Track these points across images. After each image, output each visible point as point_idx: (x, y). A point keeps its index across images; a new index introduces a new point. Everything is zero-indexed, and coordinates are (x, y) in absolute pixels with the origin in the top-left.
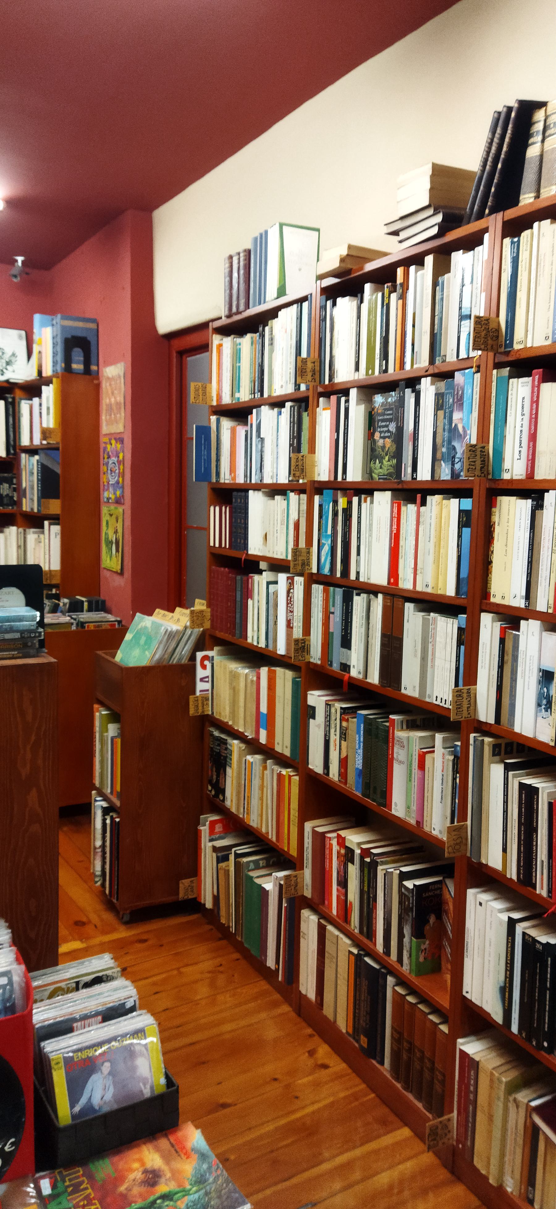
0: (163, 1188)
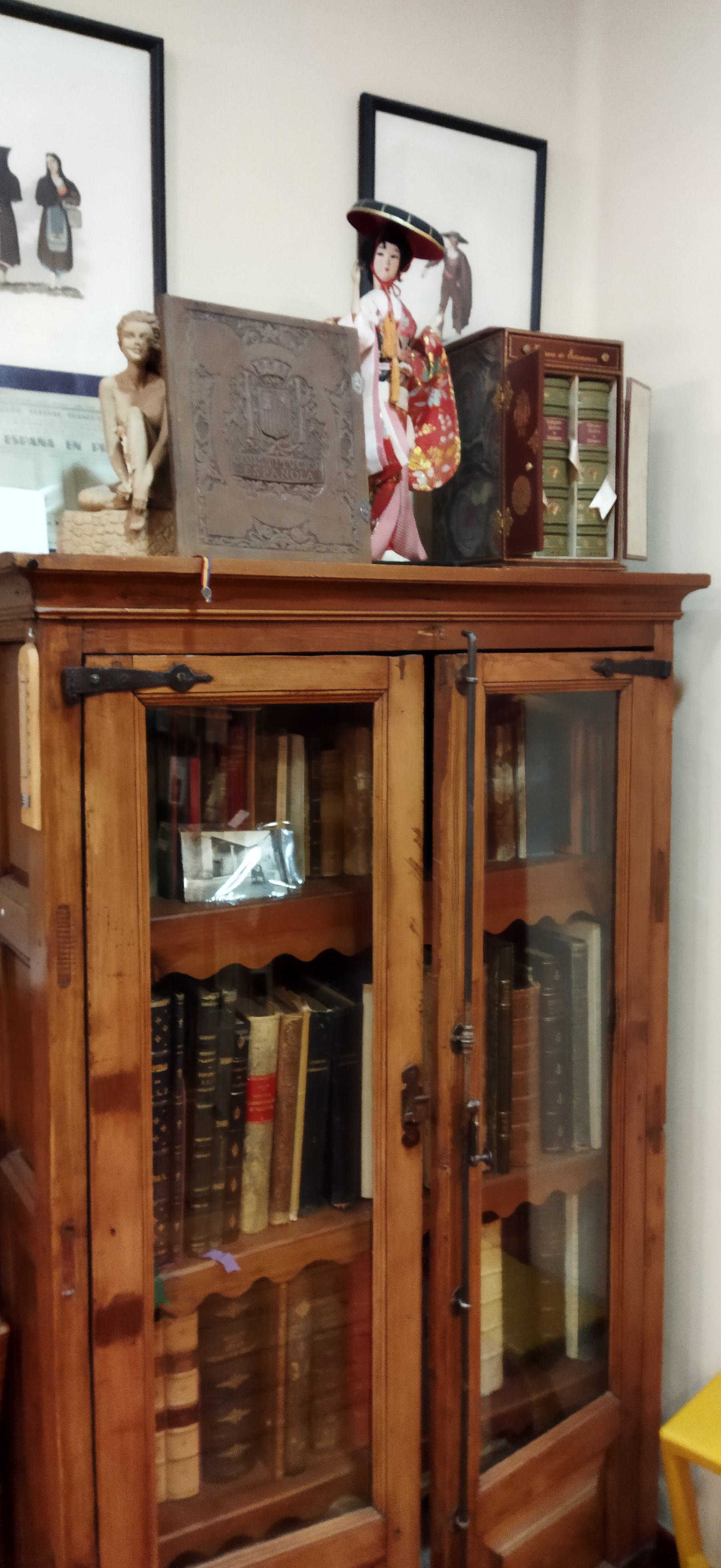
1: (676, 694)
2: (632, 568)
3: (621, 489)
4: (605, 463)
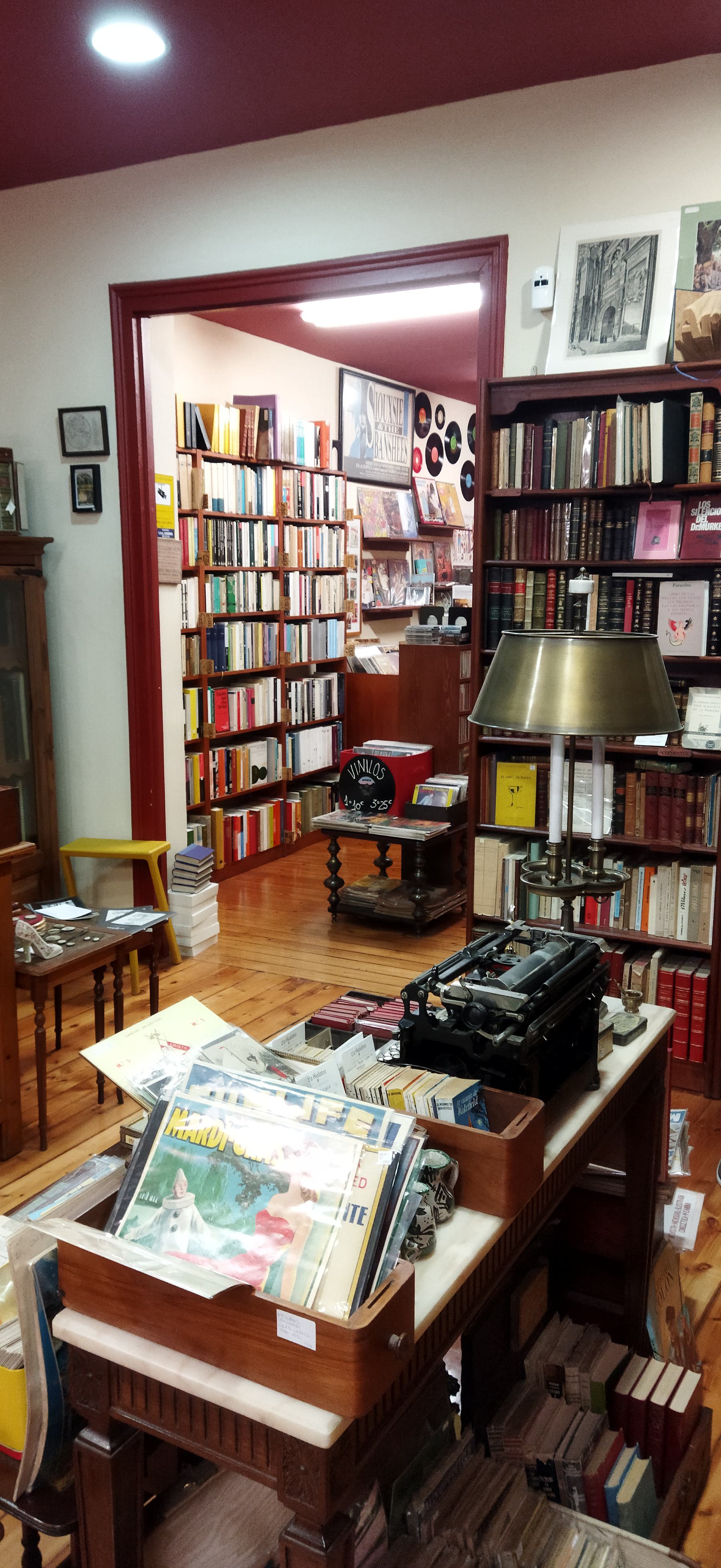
1: (44, 584)
2: (24, 534)
3: (17, 504)
4: (9, 494)
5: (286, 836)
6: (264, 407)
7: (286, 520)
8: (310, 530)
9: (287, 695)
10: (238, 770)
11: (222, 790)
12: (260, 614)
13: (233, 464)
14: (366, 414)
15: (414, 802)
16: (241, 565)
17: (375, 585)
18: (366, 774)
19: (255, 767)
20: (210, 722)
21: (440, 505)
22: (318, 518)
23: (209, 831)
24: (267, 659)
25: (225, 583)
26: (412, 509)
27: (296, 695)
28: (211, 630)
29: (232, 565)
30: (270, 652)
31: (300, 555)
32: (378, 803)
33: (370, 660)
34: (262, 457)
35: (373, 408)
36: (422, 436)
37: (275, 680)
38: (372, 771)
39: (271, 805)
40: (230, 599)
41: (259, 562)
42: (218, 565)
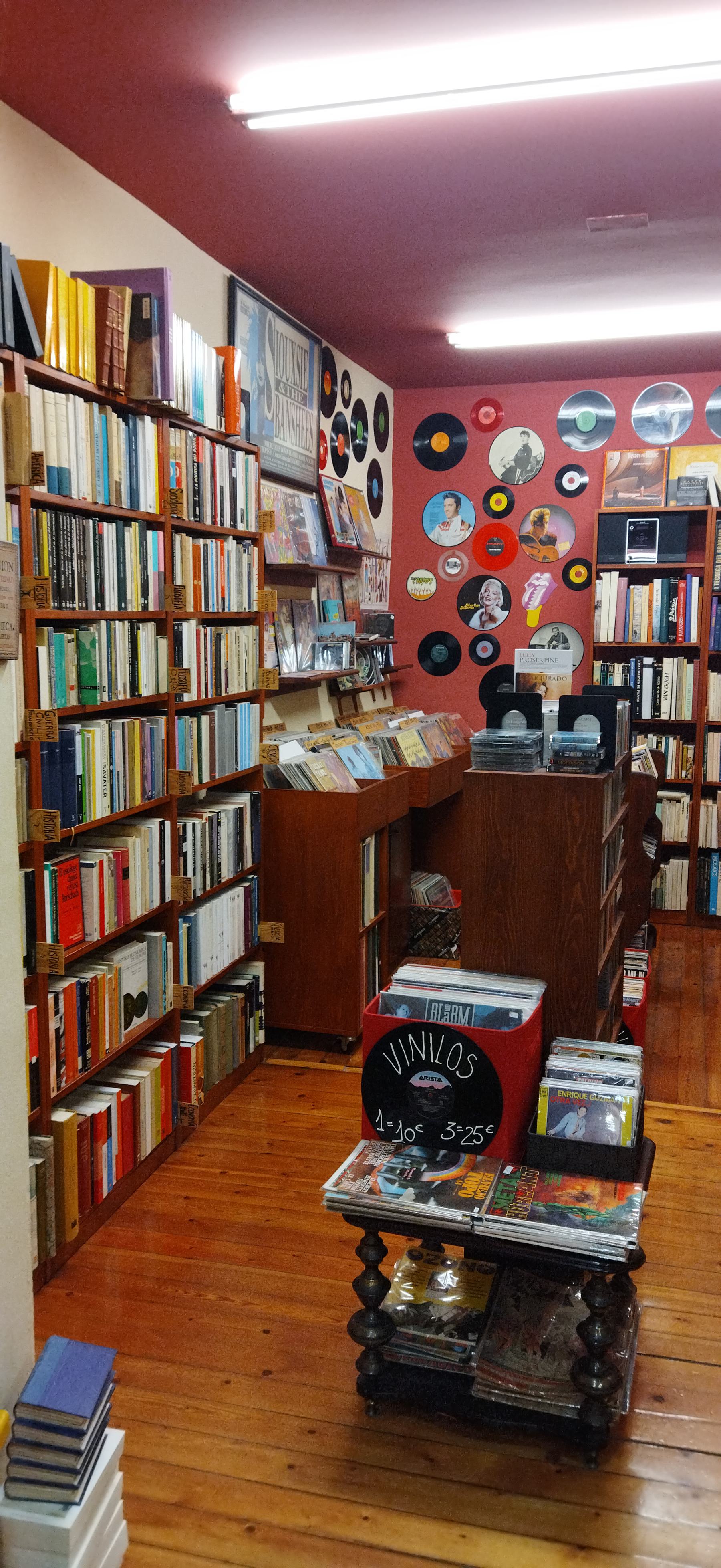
0: (585, 1205)
5: (182, 1112)
6: (142, 290)
7: (176, 522)
8: (212, 544)
9: (181, 848)
10: (101, 1016)
11: (72, 1067)
12: (139, 702)
13: (87, 400)
14: (264, 362)
15: (542, 1128)
16: (103, 607)
17: (278, 638)
18: (427, 1065)
19: (128, 996)
20: (49, 940)
21: (351, 519)
22: (222, 524)
23: (51, 1171)
24: (148, 787)
25: (73, 644)
26: (319, 524)
27: (194, 845)
28: (51, 746)
29: (87, 608)
30: (152, 773)
31: (196, 588)
32: (460, 1129)
33: (298, 766)
34: (139, 394)
35: (273, 355)
36: (328, 416)
37: (162, 824)
38: (443, 1058)
39: (157, 1062)
40: (85, 676)
41: (134, 604)
42: (60, 608)
